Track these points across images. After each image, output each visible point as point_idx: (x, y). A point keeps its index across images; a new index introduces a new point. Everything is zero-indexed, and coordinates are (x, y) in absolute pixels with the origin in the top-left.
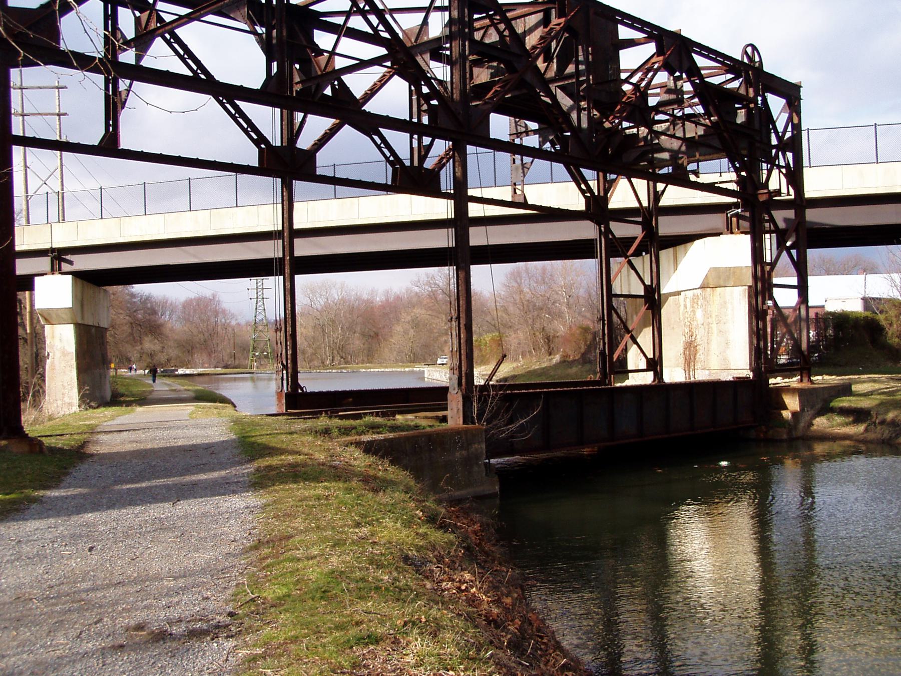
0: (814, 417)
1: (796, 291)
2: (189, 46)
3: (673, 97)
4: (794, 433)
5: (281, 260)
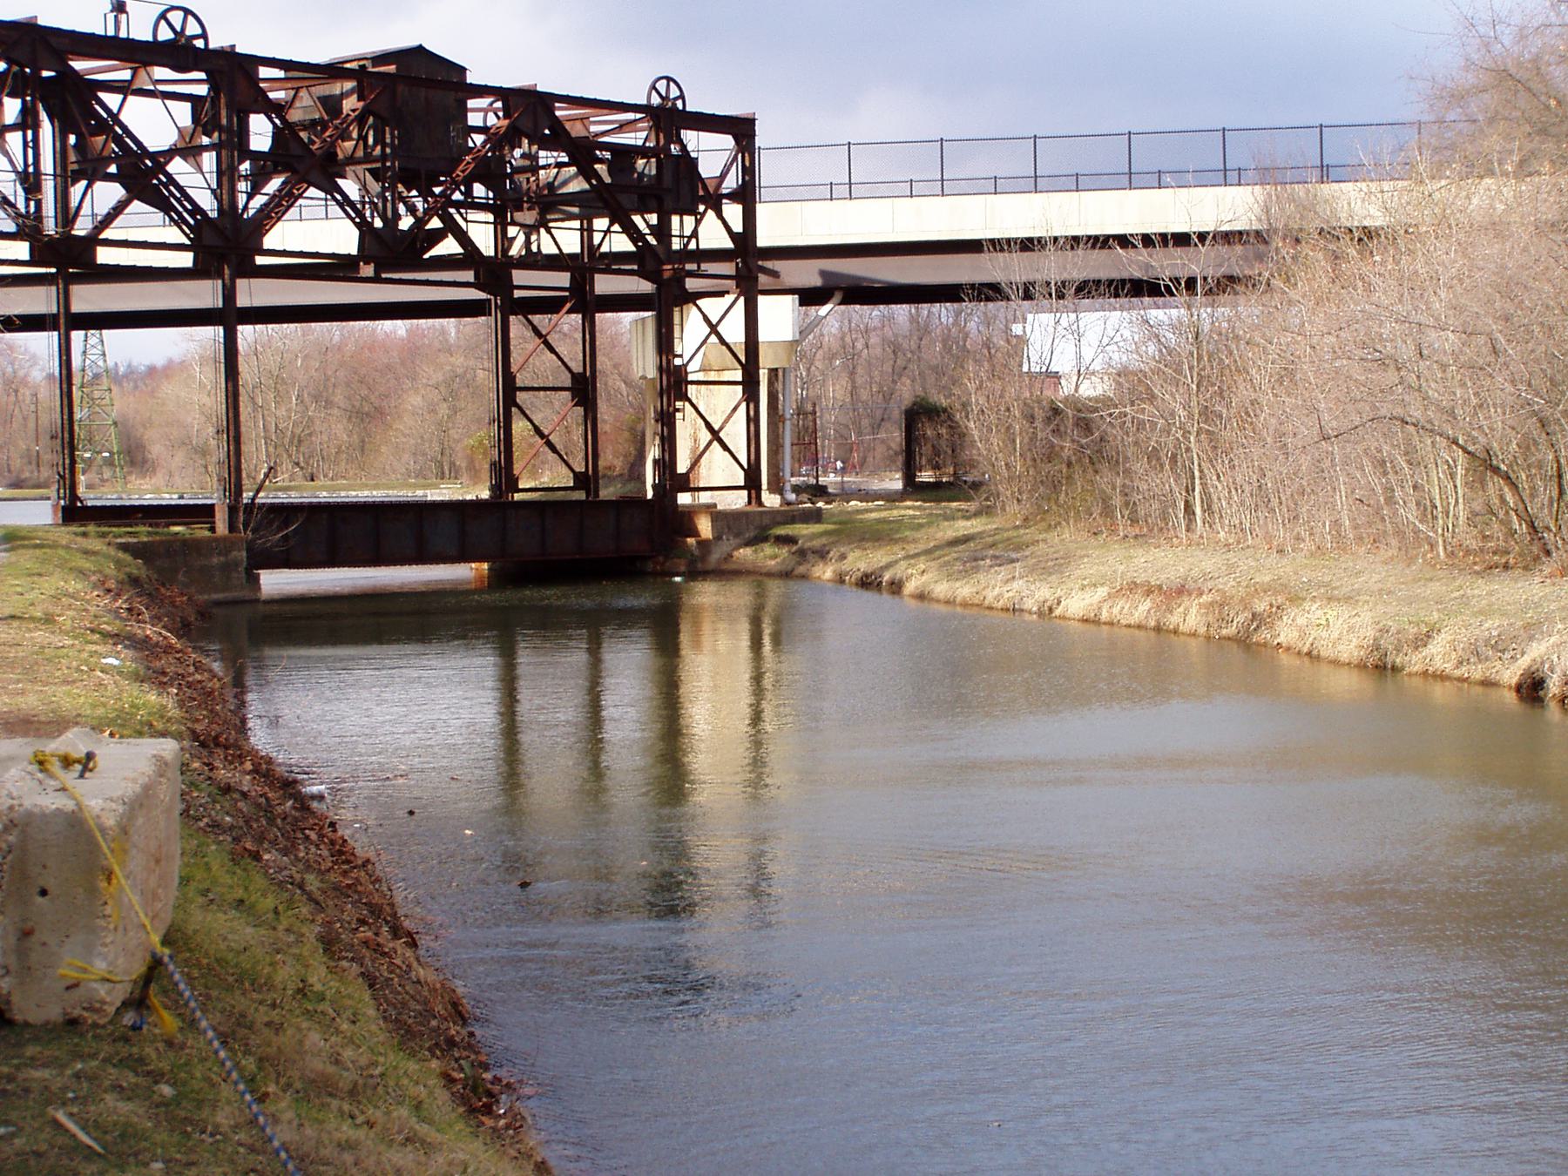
0: (738, 548)
1: (740, 388)
2: (78, 29)
3: (527, 163)
4: (699, 565)
5: (55, 317)
